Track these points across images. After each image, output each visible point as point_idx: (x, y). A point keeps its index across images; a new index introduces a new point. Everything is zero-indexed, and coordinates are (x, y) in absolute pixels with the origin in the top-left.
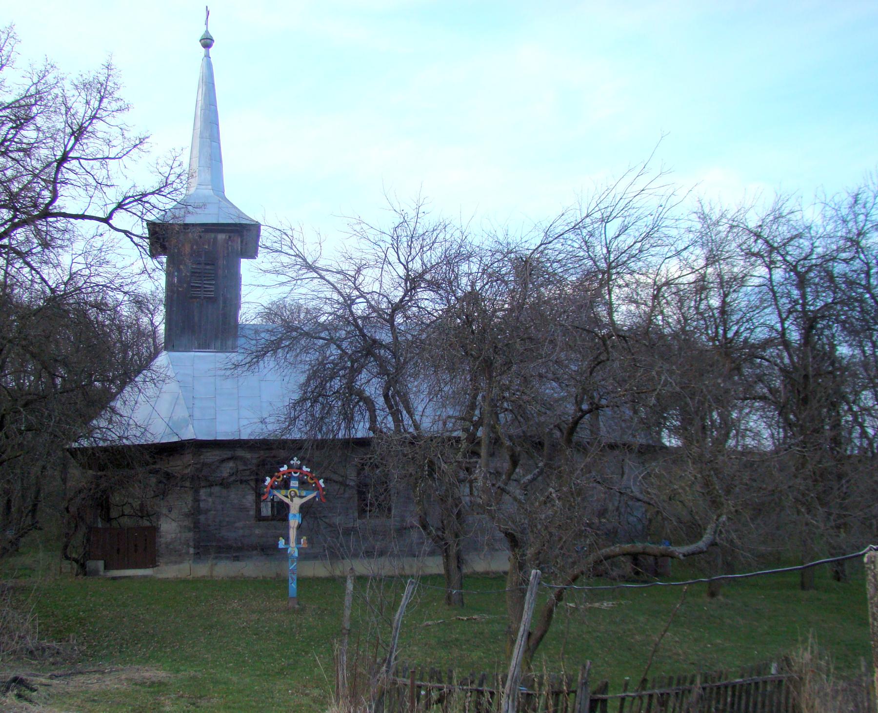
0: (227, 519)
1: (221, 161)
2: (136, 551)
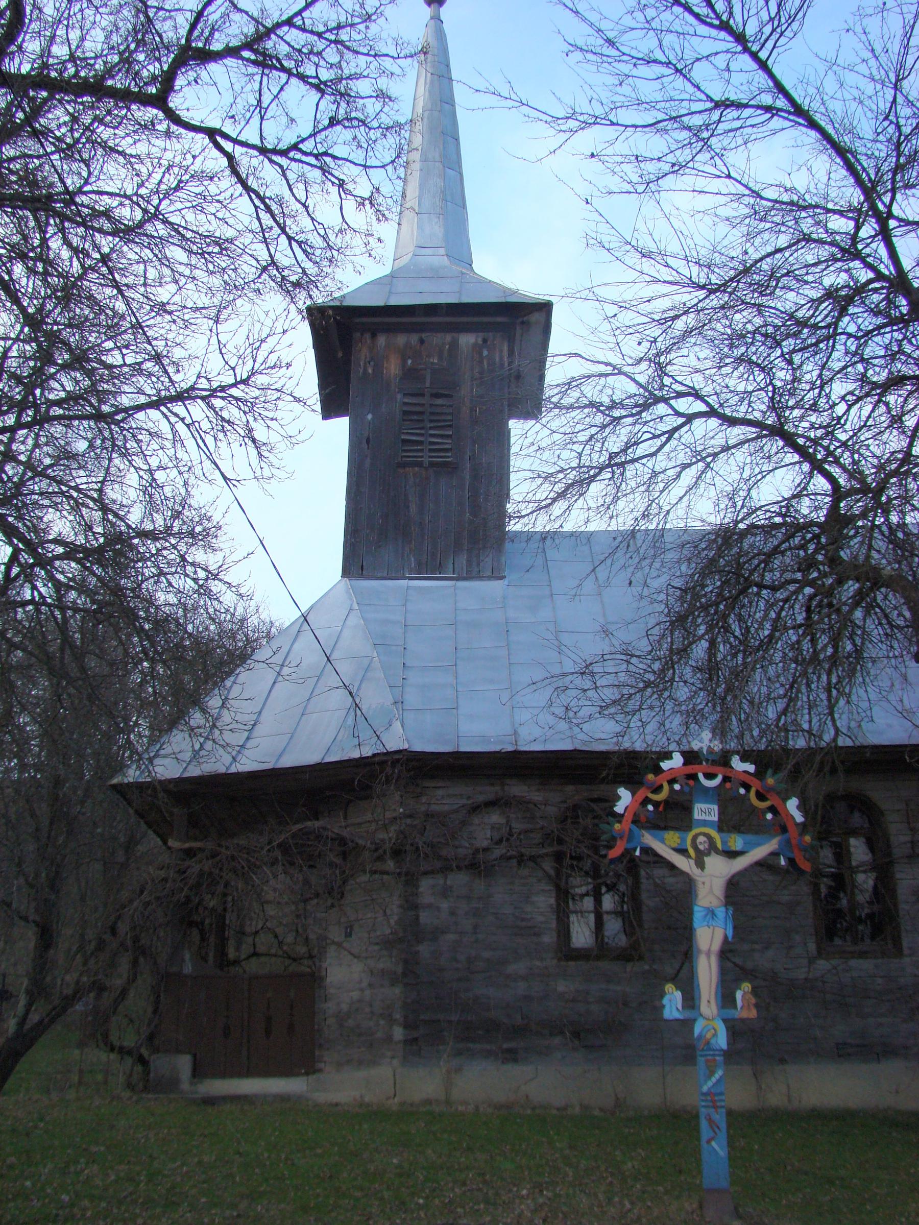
0: (486, 954)
1: (464, 206)
2: (268, 1032)
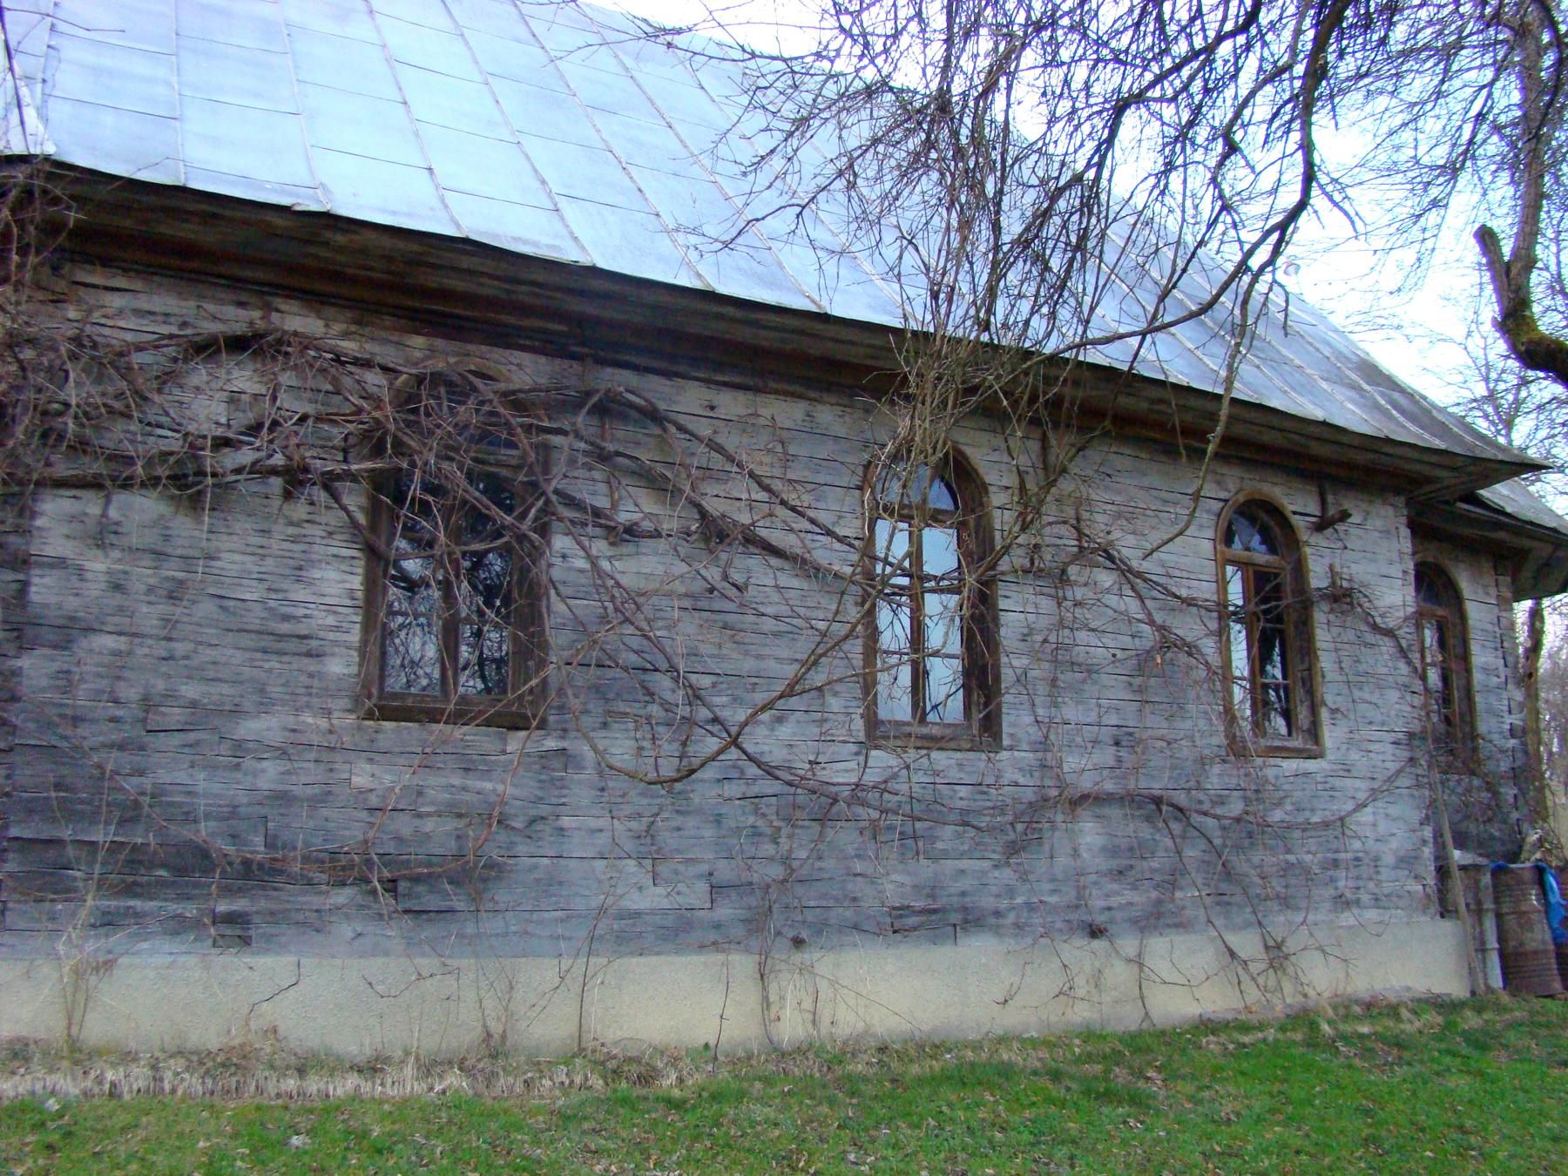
0: (190, 691)
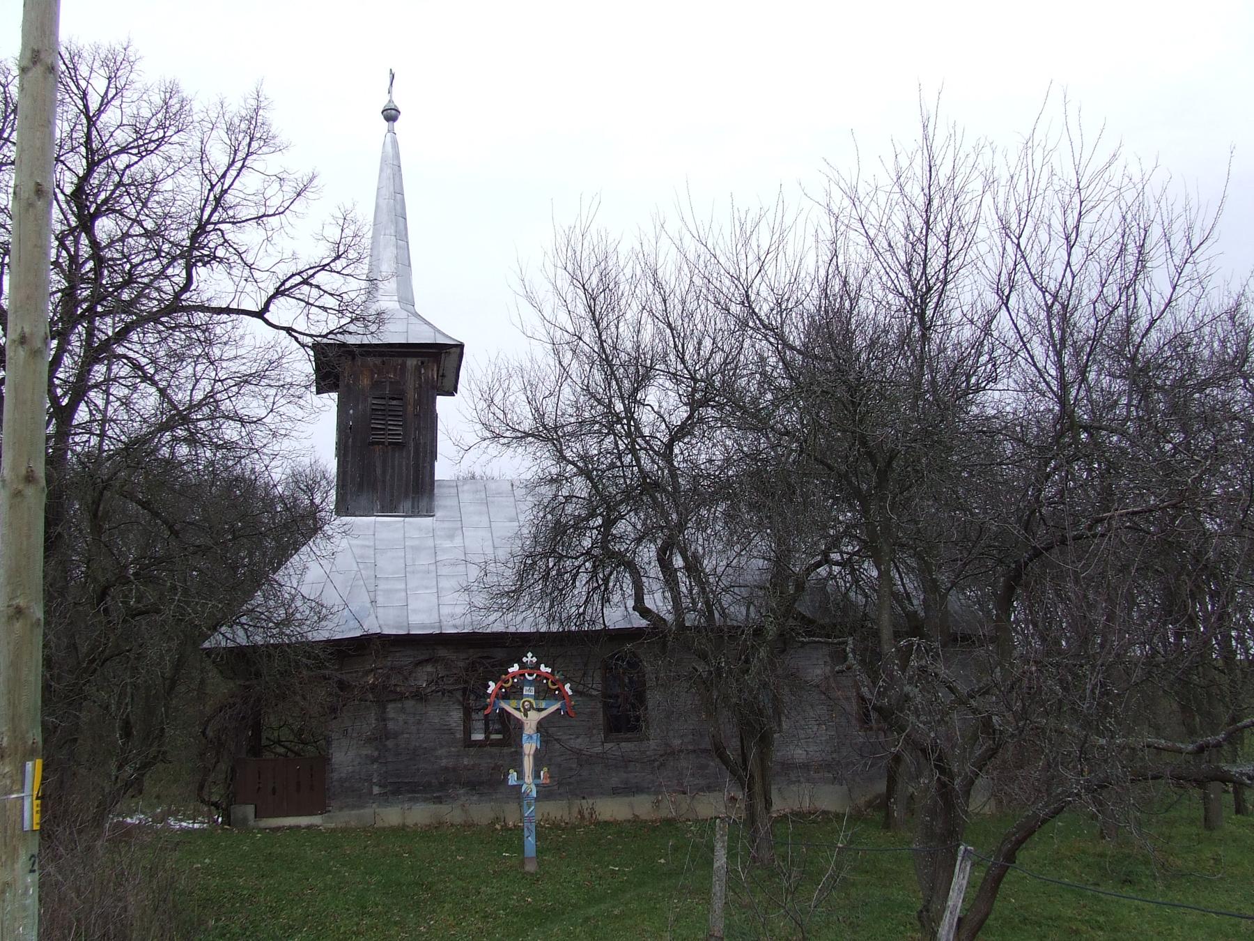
1: (410, 265)
